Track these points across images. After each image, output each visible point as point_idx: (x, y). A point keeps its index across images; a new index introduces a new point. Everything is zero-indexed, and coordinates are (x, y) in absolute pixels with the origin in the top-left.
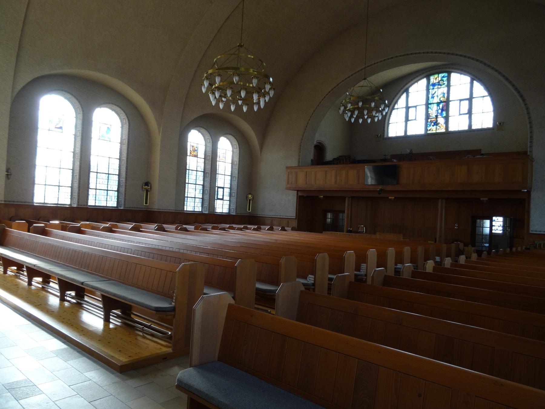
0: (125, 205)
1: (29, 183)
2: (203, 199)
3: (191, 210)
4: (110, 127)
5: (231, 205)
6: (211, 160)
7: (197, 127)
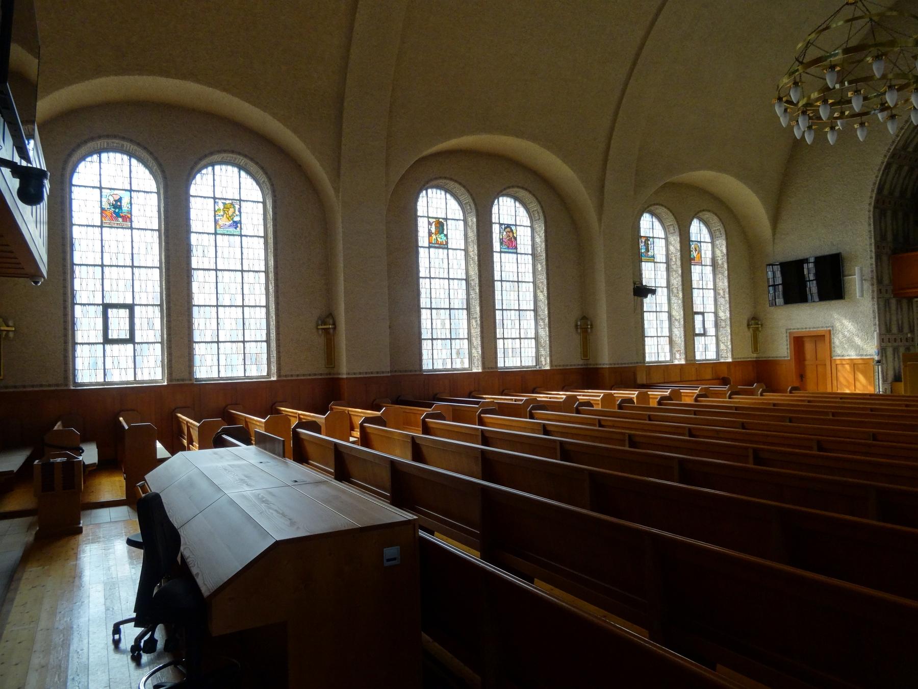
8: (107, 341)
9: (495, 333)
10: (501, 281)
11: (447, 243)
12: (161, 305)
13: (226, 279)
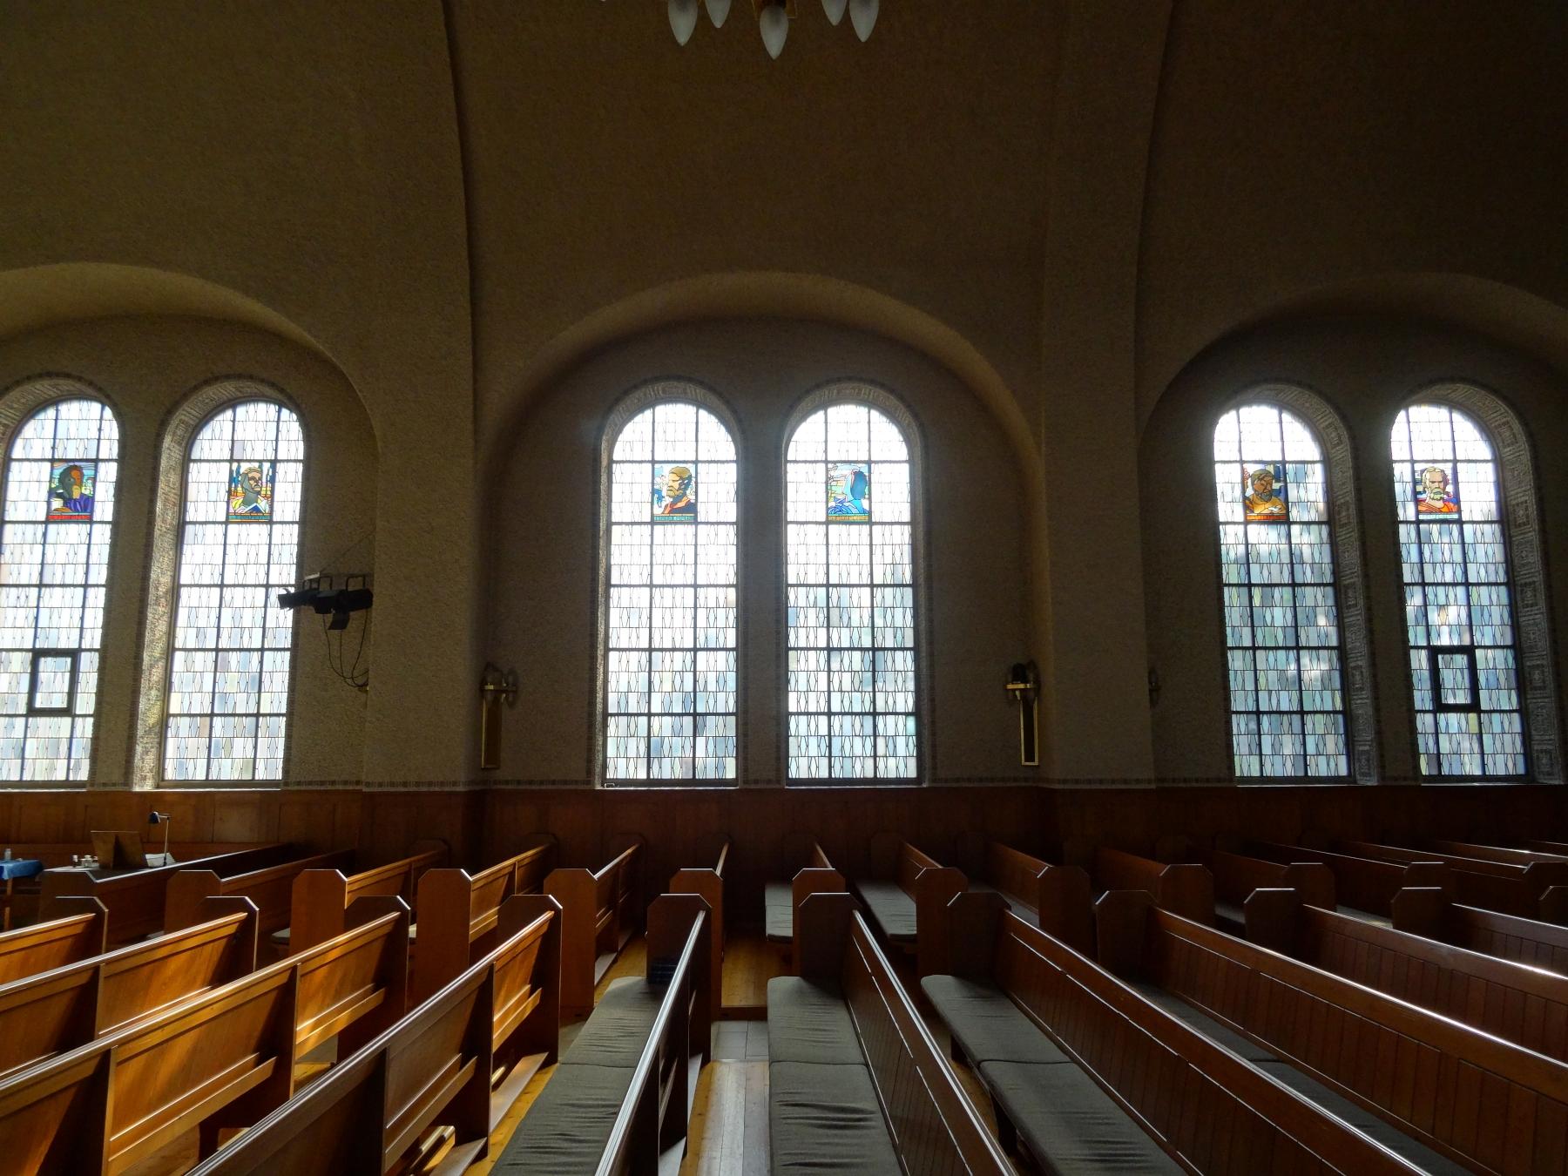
0: (934, 768)
1: (585, 718)
2: (1347, 713)
3: (679, 774)
4: (864, 468)
5: (294, 752)
6: (1365, 518)
7: (1432, 382)
8: (32, 711)
9: (1411, 698)
10: (1423, 584)
12: (607, 650)
13: (1310, 602)
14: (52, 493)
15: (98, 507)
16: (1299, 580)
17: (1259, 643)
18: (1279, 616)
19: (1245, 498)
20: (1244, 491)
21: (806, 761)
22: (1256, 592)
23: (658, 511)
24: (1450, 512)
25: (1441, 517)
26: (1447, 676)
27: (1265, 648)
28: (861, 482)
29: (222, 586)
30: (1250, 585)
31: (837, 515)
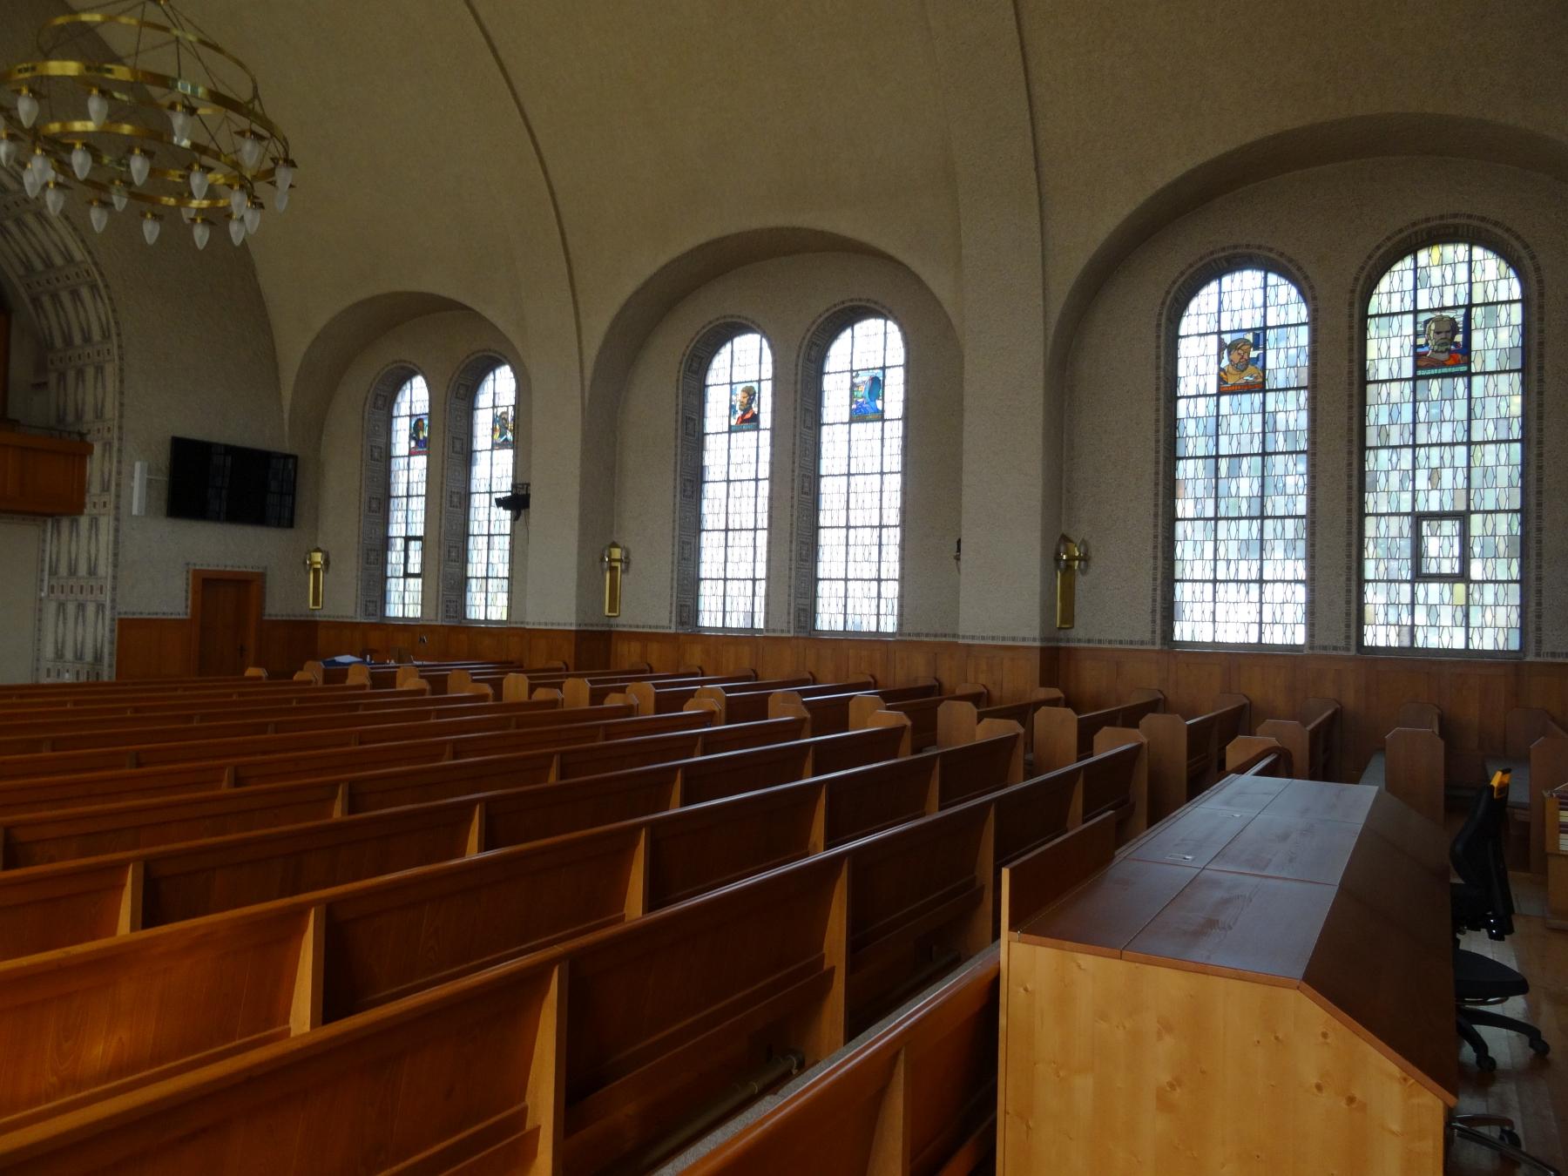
4: (879, 374)
11: (1264, 383)
13: (1280, 470)
14: (411, 437)
15: (762, 417)
16: (1269, 449)
17: (1222, 513)
18: (1247, 486)
19: (1221, 370)
20: (1219, 362)
21: (829, 618)
22: (1223, 463)
23: (733, 422)
24: (1457, 364)
25: (1445, 370)
26: (1432, 546)
27: (1228, 519)
28: (877, 385)
29: (849, 475)
30: (1217, 457)
31: (859, 415)
